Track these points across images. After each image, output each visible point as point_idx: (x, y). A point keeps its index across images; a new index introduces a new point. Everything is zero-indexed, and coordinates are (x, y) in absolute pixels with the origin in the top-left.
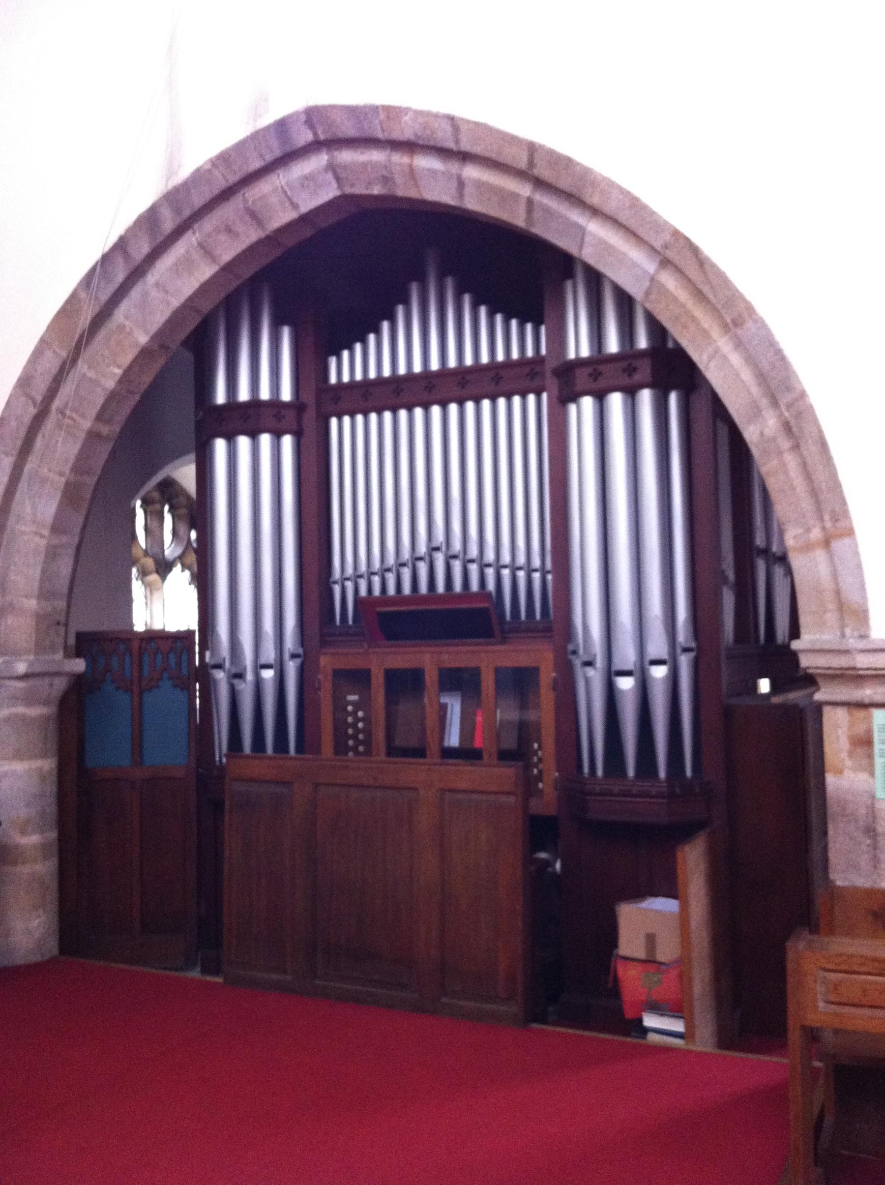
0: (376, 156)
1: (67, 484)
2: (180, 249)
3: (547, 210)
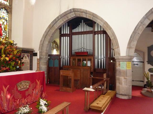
0: (79, 13)
1: (49, 41)
2: (60, 20)
3: (94, 18)
